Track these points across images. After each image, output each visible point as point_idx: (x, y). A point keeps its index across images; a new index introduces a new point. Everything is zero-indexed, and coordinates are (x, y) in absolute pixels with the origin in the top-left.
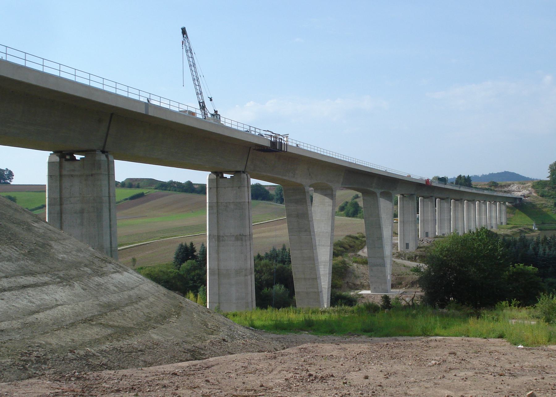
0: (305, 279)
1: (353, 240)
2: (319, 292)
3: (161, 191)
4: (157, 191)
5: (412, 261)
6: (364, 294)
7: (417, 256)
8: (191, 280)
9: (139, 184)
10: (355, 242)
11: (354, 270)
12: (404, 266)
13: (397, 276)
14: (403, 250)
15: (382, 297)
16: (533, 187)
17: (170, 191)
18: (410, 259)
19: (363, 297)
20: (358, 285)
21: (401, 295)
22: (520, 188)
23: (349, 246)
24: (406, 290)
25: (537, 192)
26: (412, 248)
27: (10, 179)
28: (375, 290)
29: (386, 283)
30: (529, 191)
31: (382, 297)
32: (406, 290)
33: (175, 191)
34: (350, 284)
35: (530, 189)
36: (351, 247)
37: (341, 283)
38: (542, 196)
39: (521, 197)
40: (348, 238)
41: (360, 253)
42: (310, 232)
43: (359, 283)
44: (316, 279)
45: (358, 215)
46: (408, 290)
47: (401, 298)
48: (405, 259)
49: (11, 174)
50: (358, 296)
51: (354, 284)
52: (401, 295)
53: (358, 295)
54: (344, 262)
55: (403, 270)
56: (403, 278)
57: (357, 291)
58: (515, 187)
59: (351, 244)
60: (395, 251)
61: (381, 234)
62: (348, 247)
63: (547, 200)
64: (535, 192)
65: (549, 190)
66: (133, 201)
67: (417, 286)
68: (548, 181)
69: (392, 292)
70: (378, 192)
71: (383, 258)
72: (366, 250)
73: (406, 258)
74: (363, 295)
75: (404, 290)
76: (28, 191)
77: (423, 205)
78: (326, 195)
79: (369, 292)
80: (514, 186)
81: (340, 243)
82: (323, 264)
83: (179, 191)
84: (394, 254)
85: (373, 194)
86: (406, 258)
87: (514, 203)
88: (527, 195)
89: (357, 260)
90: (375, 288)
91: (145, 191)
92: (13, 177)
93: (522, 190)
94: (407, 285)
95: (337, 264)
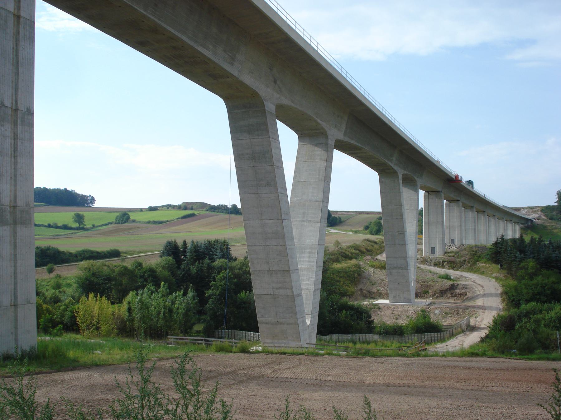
0: (270, 272)
1: (371, 243)
2: (293, 295)
3: (211, 212)
4: (207, 212)
5: (440, 267)
6: (381, 304)
7: (445, 261)
8: (141, 277)
9: (192, 206)
10: (373, 246)
11: (369, 275)
12: (431, 272)
13: (422, 283)
14: (428, 255)
15: (503, 236)
16: (542, 211)
17: (218, 212)
18: (436, 265)
19: (379, 308)
20: (374, 293)
21: (428, 307)
22: (530, 212)
23: (367, 249)
24: (434, 300)
25: (545, 215)
26: (439, 253)
27: (92, 203)
28: (395, 299)
29: (409, 291)
30: (539, 214)
31: (503, 236)
32: (434, 300)
33: (222, 212)
34: (365, 291)
35: (539, 213)
36: (368, 251)
37: (353, 290)
38: (551, 219)
39: (533, 219)
40: (365, 242)
41: (379, 257)
42: (276, 186)
43: (375, 290)
44: (288, 271)
45: (381, 233)
46: (436, 300)
47: (429, 310)
48: (431, 265)
49: (93, 200)
50: (373, 306)
51: (369, 292)
52: (428, 307)
53: (373, 305)
54: (358, 266)
55: (430, 276)
56: (430, 285)
57: (372, 300)
58: (525, 211)
59: (369, 248)
60: (419, 256)
61: (403, 228)
62: (365, 251)
63: (556, 222)
64: (544, 216)
65: (557, 213)
66: (184, 219)
67: (447, 296)
68: (556, 206)
69: (416, 302)
70: (401, 172)
71: (405, 258)
72: (384, 255)
73: (432, 264)
74: (380, 305)
75: (432, 301)
76: (100, 212)
77: (449, 211)
78: (316, 145)
79: (387, 302)
80: (524, 210)
81: (355, 245)
82: (308, 250)
83: (226, 213)
84: (417, 259)
85: (394, 173)
86: (432, 264)
87: (526, 225)
88: (537, 218)
89: (374, 264)
90: (394, 297)
91: (196, 212)
92: (95, 202)
93: (531, 214)
94: (435, 294)
95: (349, 268)
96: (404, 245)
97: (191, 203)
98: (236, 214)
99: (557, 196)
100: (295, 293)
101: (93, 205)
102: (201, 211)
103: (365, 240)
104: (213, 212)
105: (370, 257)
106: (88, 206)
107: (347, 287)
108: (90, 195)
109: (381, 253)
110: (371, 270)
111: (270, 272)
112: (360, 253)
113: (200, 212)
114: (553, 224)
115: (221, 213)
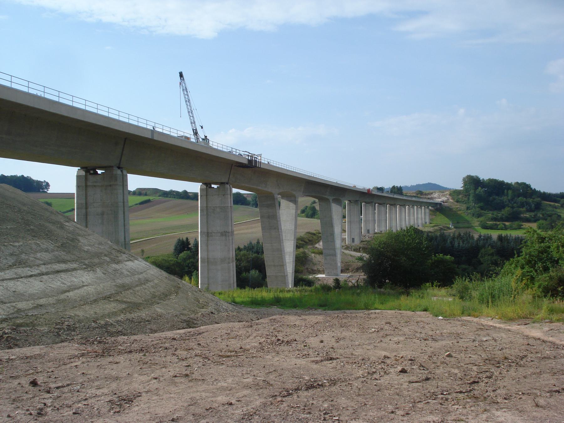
0: (274, 266)
5: (357, 252)
9: (146, 192)
10: (313, 237)
12: (351, 256)
16: (450, 195)
17: (170, 197)
18: (355, 250)
19: (319, 280)
20: (315, 270)
22: (440, 196)
23: (309, 240)
25: (453, 199)
26: (357, 242)
27: (47, 188)
28: (328, 274)
29: (337, 269)
30: (447, 198)
36: (310, 241)
37: (302, 269)
38: (457, 202)
39: (441, 203)
41: (317, 245)
44: (283, 265)
45: (316, 217)
46: (354, 274)
48: (351, 251)
49: (48, 185)
51: (312, 270)
53: (315, 278)
54: (304, 253)
55: (350, 259)
56: (350, 265)
59: (310, 239)
60: (343, 244)
62: (308, 241)
63: (461, 204)
64: (451, 199)
68: (462, 190)
69: (342, 276)
70: (331, 198)
71: (334, 249)
72: (321, 243)
76: (61, 198)
78: (290, 201)
79: (324, 276)
89: (315, 251)
90: (328, 273)
92: (50, 187)
96: (333, 241)
97: (145, 189)
98: (187, 199)
99: (463, 182)
100: (286, 275)
101: (48, 190)
102: (154, 196)
103: (307, 233)
104: (166, 197)
105: (311, 246)
106: (43, 192)
107: (299, 267)
108: (45, 181)
109: (319, 242)
110: (313, 255)
111: (274, 266)
112: (305, 244)
113: (154, 197)
114: (458, 207)
115: (173, 199)
